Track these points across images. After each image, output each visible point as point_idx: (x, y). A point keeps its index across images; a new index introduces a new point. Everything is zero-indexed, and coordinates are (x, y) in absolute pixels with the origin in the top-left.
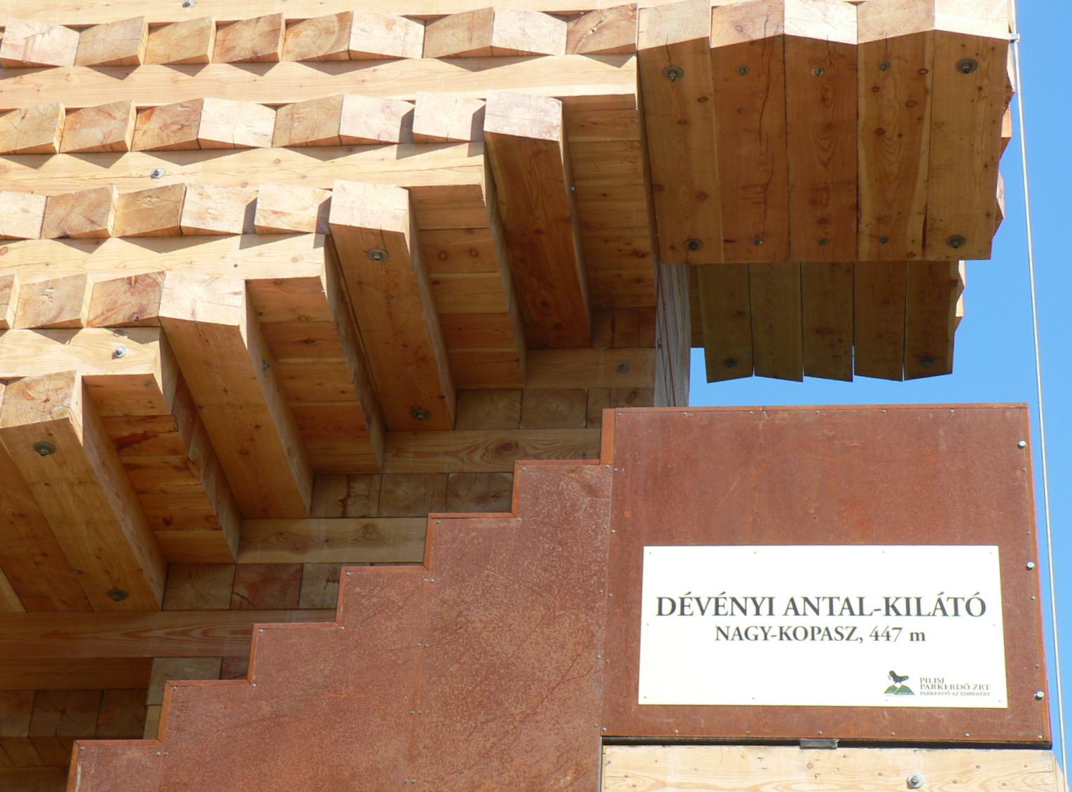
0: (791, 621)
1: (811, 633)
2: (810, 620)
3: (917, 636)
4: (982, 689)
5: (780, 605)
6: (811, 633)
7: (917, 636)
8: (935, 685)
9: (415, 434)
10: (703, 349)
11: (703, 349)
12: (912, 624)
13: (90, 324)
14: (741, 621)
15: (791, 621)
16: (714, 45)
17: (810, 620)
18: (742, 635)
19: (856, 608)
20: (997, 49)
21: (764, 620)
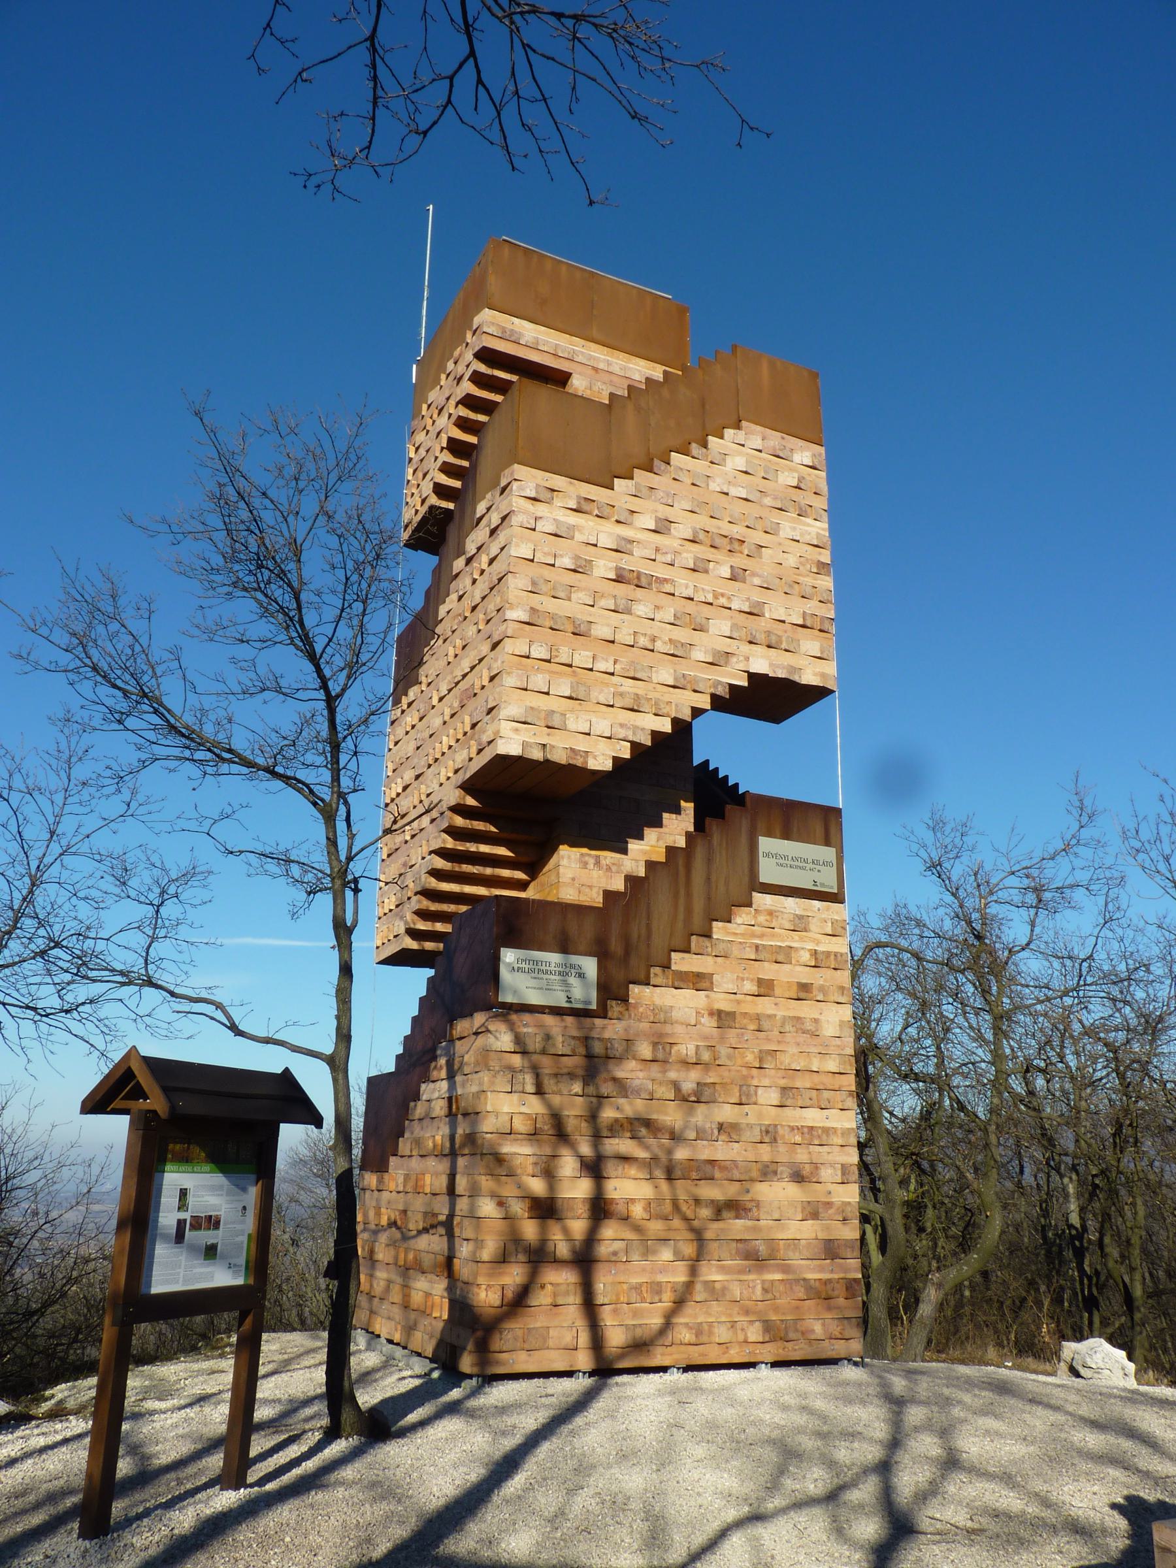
0: (792, 863)
1: (797, 867)
2: (796, 863)
3: (819, 871)
4: (832, 887)
5: (790, 858)
6: (797, 867)
7: (819, 871)
8: (822, 885)
9: (571, 1079)
10: (282, 1126)
11: (282, 1126)
12: (818, 867)
13: (693, 719)
14: (781, 861)
15: (792, 863)
16: (691, 829)
17: (796, 863)
18: (781, 865)
19: (806, 861)
20: (564, 388)
21: (786, 862)
